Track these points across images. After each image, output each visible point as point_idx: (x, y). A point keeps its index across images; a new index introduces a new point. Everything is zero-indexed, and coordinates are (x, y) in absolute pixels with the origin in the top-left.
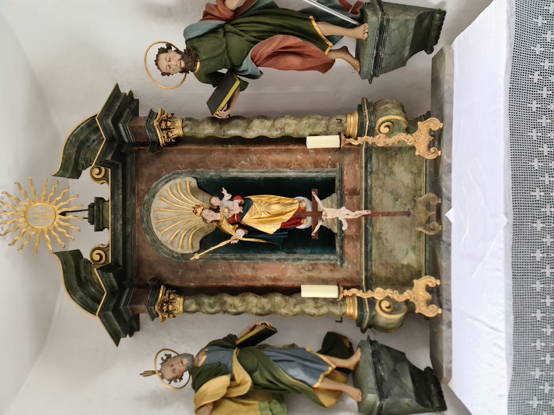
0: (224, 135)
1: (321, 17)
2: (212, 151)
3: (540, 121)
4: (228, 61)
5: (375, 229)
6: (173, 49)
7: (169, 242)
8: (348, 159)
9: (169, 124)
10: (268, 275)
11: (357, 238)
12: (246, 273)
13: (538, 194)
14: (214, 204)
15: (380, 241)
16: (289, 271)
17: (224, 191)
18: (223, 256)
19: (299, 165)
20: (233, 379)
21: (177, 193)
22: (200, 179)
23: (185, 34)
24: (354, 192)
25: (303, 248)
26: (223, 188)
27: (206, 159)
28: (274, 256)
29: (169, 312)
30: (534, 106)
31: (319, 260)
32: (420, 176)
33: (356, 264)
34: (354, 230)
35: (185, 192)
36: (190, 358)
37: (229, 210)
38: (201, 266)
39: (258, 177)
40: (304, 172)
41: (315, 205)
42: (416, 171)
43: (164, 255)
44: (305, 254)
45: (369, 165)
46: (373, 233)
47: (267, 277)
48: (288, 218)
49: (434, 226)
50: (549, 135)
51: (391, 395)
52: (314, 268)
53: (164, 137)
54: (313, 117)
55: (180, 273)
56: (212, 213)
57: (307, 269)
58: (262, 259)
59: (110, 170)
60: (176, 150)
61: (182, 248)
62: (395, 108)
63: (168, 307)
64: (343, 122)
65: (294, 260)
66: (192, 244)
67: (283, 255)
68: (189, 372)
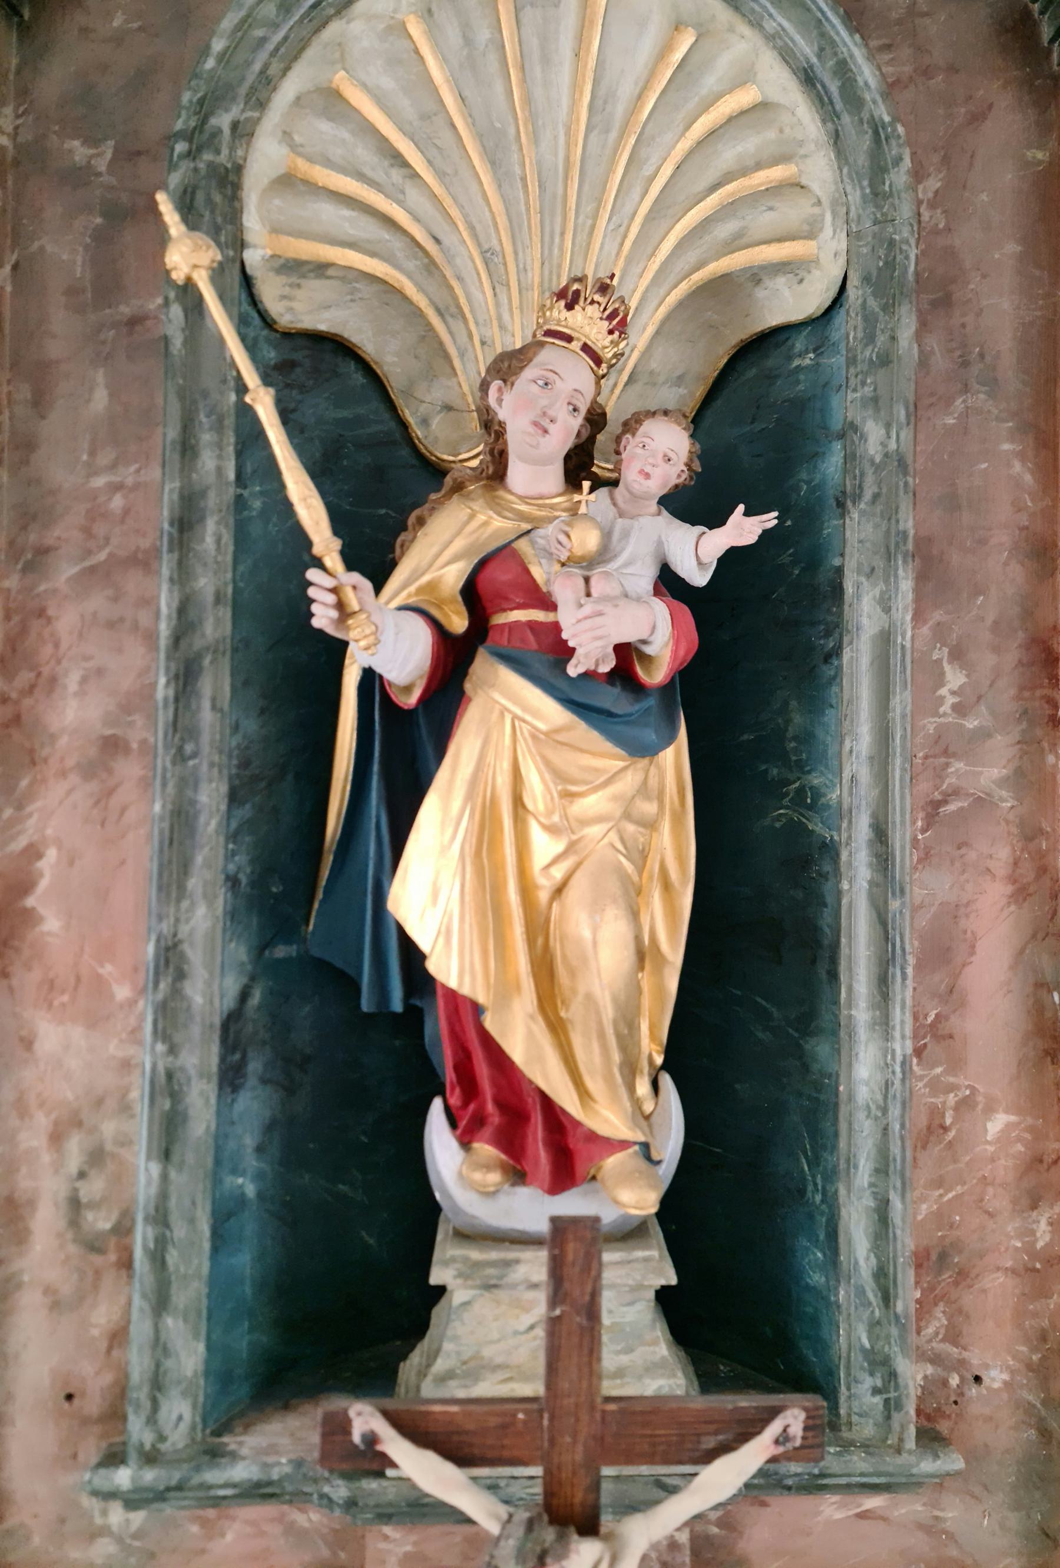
7: (340, 79)
10: (48, 863)
12: (72, 681)
14: (632, 446)
16: (77, 1033)
17: (743, 529)
18: (212, 500)
19: (935, 1128)
21: (711, 176)
25: (270, 1127)
26: (770, 520)
27: (980, 398)
28: (203, 916)
31: (161, 1303)
35: (724, 230)
37: (588, 565)
38: (134, 322)
43: (228, 23)
47: (33, 852)
48: (516, 1051)
52: (94, 1245)
55: (79, 151)
56: (565, 430)
57: (93, 1188)
58: (181, 820)
61: (288, 182)
65: (169, 1087)
66: (321, 269)
67: (212, 987)
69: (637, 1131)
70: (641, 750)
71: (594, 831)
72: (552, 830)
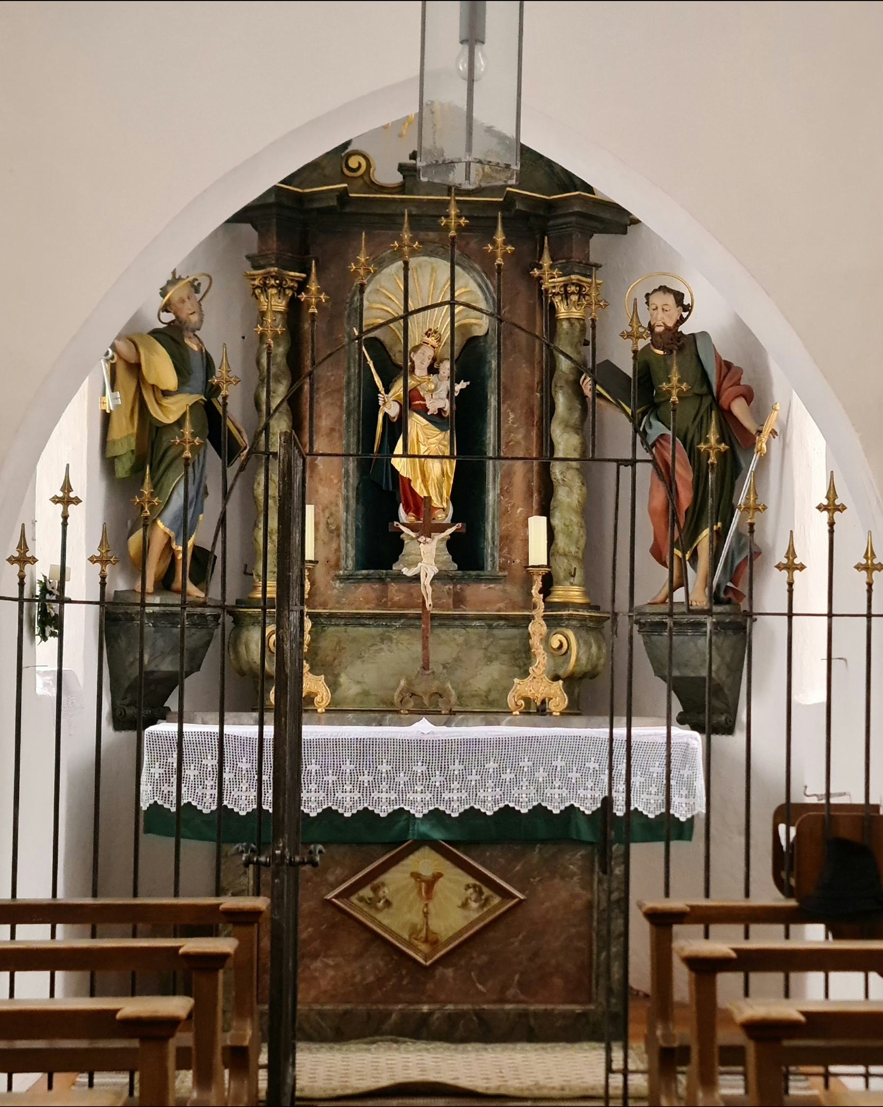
0: (556, 386)
1: (720, 537)
2: (531, 363)
3: (541, 769)
4: (663, 400)
5: (398, 632)
6: (685, 315)
8: (514, 591)
9: (574, 298)
11: (382, 600)
12: (324, 416)
13: (457, 767)
15: (378, 639)
20: (166, 393)
22: (486, 342)
23: (704, 334)
24: (459, 600)
26: (468, 383)
29: (264, 287)
30: (559, 763)
31: (347, 542)
32: (482, 704)
33: (338, 602)
34: (396, 599)
36: (197, 325)
39: (487, 442)
40: (493, 518)
41: (441, 528)
42: (490, 698)
44: (356, 519)
45: (502, 623)
46: (390, 629)
48: (418, 490)
49: (407, 702)
50: (524, 779)
51: (156, 632)
52: (332, 532)
53: (554, 287)
54: (582, 533)
59: (501, 199)
60: (534, 304)
62: (589, 659)
63: (273, 286)
64: (572, 580)
65: (346, 499)
67: (353, 480)
68: (173, 322)
69: (443, 509)
70: (442, 430)
71: (433, 446)
72: (425, 445)
